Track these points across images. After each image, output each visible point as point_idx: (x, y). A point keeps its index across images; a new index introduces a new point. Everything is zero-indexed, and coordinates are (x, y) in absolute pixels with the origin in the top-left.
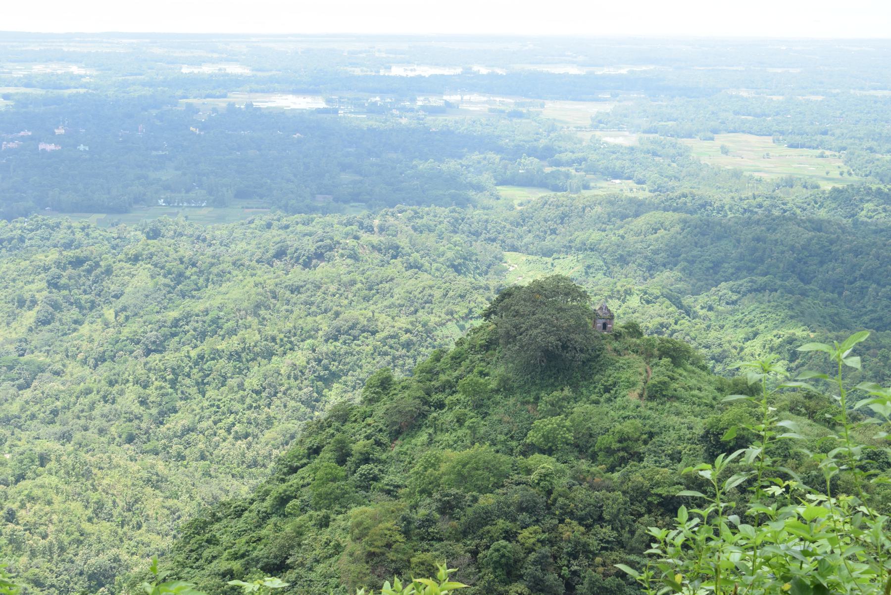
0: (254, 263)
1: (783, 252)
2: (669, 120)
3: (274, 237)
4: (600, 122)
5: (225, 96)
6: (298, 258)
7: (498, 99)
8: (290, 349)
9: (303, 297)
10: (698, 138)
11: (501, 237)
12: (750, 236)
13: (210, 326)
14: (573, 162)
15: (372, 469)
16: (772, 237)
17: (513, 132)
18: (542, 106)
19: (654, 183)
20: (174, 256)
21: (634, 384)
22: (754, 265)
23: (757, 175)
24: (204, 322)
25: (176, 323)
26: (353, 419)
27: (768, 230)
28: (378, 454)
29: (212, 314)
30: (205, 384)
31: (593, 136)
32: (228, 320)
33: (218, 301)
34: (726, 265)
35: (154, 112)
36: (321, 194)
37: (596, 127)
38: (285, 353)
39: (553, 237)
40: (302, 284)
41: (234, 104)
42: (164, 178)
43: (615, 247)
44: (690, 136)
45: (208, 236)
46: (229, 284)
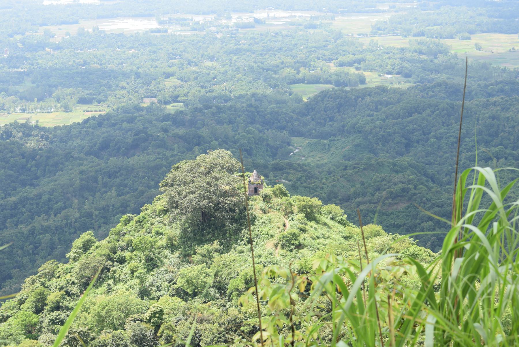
0: (82, 155)
1: (513, 127)
2: (434, 25)
3: (103, 133)
4: (379, 29)
5: (76, 22)
6: (119, 149)
7: (297, 15)
8: (104, 223)
9: (118, 180)
10: (457, 39)
11: (289, 125)
12: (487, 115)
13: (42, 207)
14: (355, 62)
15: (59, 315)
16: (504, 115)
17: (307, 40)
18: (333, 18)
19: (418, 76)
20: (17, 152)
21: (272, 236)
22: (490, 138)
23: (502, 67)
24: (38, 204)
25: (15, 206)
26: (58, 275)
27: (503, 109)
28: (69, 303)
29: (45, 197)
30: (35, 254)
31: (372, 41)
32: (57, 203)
33: (51, 186)
34: (467, 140)
35: (18, 37)
36: (148, 97)
37: (375, 33)
38: (100, 227)
39: (331, 123)
40: (117, 170)
41: (83, 29)
42: (21, 91)
43: (378, 129)
44: (451, 37)
45: (50, 136)
46: (61, 172)
